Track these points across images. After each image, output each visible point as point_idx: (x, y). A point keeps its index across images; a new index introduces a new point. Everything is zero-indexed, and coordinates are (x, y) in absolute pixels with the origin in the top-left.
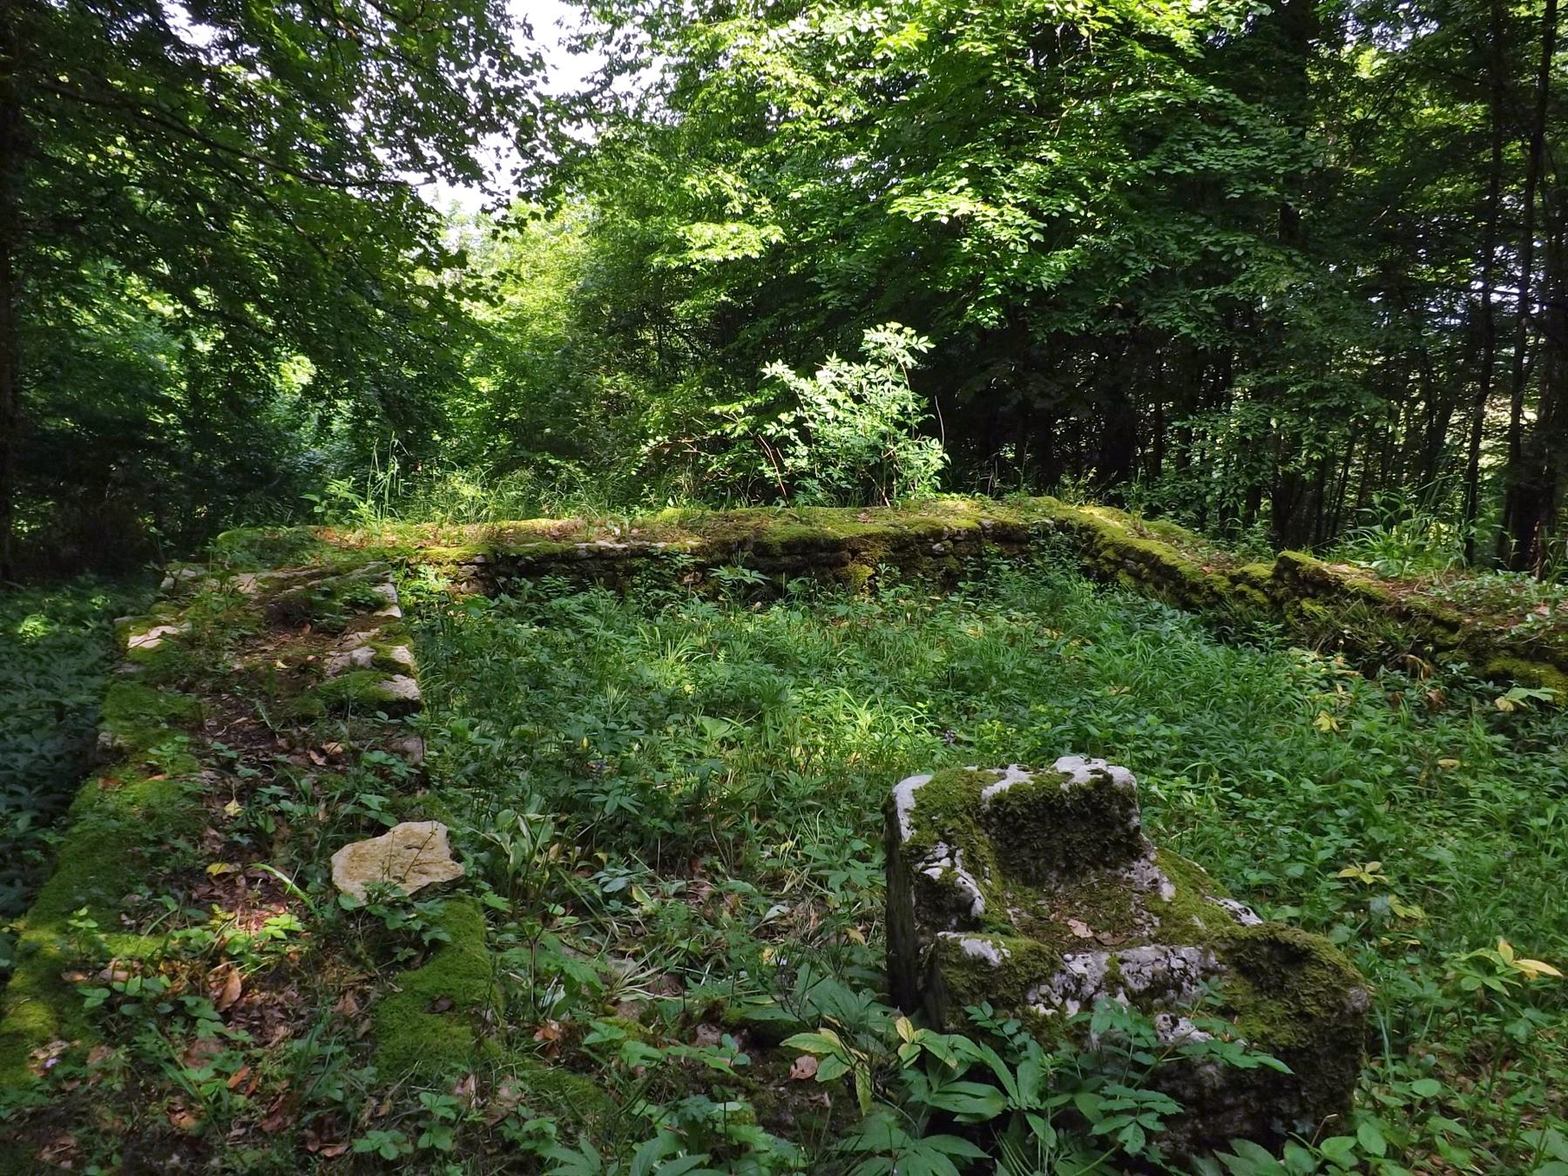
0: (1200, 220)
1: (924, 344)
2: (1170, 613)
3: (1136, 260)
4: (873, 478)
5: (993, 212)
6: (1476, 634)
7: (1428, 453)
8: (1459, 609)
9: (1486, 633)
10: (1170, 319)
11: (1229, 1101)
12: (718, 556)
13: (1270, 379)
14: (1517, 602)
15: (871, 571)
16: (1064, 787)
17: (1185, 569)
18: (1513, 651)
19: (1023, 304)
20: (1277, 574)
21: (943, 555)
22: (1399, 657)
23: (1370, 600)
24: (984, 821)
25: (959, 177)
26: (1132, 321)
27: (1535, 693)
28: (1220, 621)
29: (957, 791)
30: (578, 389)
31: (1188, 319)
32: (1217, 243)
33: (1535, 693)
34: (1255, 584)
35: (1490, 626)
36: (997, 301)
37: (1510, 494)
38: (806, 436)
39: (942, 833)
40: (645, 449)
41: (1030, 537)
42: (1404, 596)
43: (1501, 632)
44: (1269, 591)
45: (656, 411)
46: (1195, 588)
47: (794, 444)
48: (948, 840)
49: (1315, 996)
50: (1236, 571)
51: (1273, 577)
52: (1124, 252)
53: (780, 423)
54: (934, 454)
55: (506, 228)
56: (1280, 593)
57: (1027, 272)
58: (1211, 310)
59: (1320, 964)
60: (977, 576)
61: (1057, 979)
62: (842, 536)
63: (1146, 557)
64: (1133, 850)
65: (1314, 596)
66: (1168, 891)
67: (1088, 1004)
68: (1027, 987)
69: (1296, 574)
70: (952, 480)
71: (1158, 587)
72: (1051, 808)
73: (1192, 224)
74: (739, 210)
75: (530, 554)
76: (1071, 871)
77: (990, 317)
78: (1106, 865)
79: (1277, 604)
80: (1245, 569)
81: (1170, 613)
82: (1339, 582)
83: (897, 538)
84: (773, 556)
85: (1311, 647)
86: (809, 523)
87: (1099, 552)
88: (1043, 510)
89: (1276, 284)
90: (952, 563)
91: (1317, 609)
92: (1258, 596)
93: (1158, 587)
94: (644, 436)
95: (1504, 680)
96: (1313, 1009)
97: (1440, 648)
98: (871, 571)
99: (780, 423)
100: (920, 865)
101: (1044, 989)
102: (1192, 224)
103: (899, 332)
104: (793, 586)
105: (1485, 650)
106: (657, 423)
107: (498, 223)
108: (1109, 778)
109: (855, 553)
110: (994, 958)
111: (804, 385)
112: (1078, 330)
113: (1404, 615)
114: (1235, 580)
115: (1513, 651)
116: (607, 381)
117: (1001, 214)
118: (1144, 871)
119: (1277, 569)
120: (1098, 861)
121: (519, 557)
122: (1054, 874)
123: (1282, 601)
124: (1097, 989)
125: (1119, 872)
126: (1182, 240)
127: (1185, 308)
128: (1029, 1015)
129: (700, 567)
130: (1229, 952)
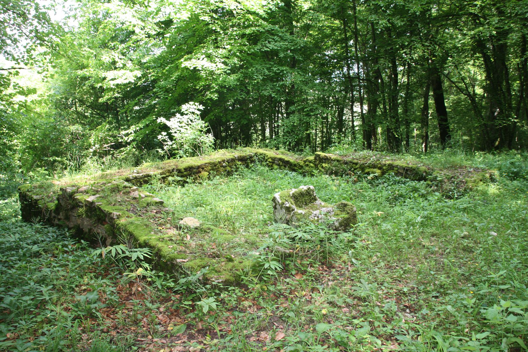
0: (272, 63)
3: (257, 76)
4: (196, 149)
5: (214, 65)
7: (340, 124)
12: (167, 174)
14: (369, 156)
18: (369, 167)
19: (224, 91)
20: (315, 159)
21: (226, 166)
22: (346, 173)
23: (338, 161)
25: (202, 55)
29: (287, 194)
31: (274, 92)
32: (278, 69)
34: (310, 162)
35: (364, 162)
36: (217, 91)
37: (364, 133)
41: (248, 158)
42: (345, 159)
44: (314, 163)
46: (295, 165)
50: (305, 159)
52: (253, 73)
53: (162, 135)
55: (47, 78)
58: (279, 89)
62: (199, 164)
63: (280, 159)
64: (316, 200)
65: (325, 162)
67: (318, 217)
70: (216, 146)
71: (285, 167)
73: (270, 64)
74: (121, 66)
76: (306, 204)
77: (215, 97)
80: (307, 158)
82: (330, 158)
83: (214, 163)
84: (182, 173)
85: (326, 174)
88: (248, 151)
89: (292, 77)
90: (228, 169)
92: (312, 165)
93: (285, 167)
94: (90, 146)
95: (368, 174)
96: (349, 212)
98: (208, 173)
99: (162, 135)
102: (270, 64)
107: (44, 77)
111: (168, 123)
112: (242, 98)
113: (346, 163)
114: (305, 162)
115: (369, 167)
117: (217, 66)
119: (315, 157)
120: (310, 202)
123: (318, 165)
126: (269, 69)
127: (271, 89)
129: (163, 178)
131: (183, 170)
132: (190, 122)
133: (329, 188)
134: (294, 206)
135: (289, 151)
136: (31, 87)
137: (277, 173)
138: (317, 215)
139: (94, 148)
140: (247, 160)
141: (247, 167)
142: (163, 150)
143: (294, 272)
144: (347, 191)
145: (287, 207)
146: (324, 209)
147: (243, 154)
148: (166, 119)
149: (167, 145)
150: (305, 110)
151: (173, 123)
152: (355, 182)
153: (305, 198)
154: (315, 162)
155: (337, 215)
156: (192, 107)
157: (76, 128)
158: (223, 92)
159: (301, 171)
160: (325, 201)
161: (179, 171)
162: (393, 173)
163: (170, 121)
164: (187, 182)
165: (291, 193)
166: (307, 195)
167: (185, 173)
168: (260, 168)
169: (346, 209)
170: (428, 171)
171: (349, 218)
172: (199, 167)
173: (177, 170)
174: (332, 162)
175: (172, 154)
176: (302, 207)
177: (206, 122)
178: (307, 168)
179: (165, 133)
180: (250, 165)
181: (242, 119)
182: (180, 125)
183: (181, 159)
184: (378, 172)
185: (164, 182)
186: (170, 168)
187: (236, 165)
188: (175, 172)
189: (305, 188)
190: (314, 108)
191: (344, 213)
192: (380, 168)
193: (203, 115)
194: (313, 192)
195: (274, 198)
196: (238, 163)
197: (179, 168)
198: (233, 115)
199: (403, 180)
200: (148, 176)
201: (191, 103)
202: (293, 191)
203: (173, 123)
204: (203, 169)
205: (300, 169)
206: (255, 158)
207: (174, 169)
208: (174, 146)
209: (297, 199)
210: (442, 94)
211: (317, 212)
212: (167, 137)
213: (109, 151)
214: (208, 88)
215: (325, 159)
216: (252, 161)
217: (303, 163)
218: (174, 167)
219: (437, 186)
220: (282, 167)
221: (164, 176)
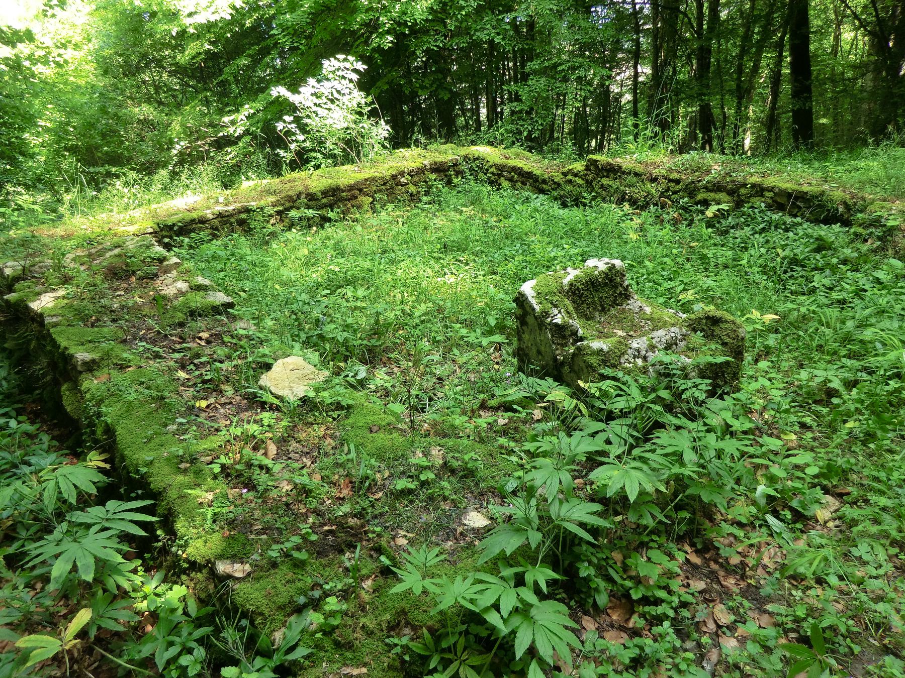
1: (366, 67)
2: (535, 196)
4: (351, 149)
6: (689, 184)
8: (679, 172)
9: (693, 182)
10: (489, 35)
12: (287, 205)
13: (546, 64)
15: (371, 199)
16: (596, 273)
17: (538, 172)
20: (587, 168)
21: (407, 184)
23: (637, 174)
26: (468, 37)
27: (721, 207)
28: (561, 197)
29: (554, 286)
31: (498, 34)
33: (721, 207)
38: (303, 129)
39: (552, 304)
40: (174, 152)
41: (449, 167)
43: (700, 181)
45: (176, 127)
46: (544, 182)
47: (294, 134)
48: (556, 306)
50: (565, 170)
51: (586, 170)
53: (284, 122)
54: (383, 130)
55: (51, 7)
57: (405, 13)
59: (727, 322)
60: (427, 193)
61: (630, 352)
62: (352, 182)
63: (513, 169)
64: (627, 297)
65: (608, 177)
66: (648, 310)
67: (645, 358)
68: (620, 357)
70: (398, 140)
72: (592, 283)
75: (179, 222)
76: (603, 310)
78: (617, 305)
79: (589, 183)
80: (570, 167)
81: (535, 196)
82: (620, 168)
84: (317, 200)
86: (330, 177)
87: (487, 170)
90: (412, 188)
91: (610, 183)
92: (579, 181)
93: (523, 183)
95: (706, 203)
96: (728, 340)
98: (371, 199)
100: (549, 319)
101: (626, 356)
103: (345, 60)
106: (178, 133)
108: (613, 265)
109: (360, 190)
110: (606, 348)
112: (438, 46)
113: (654, 180)
115: (707, 189)
116: (137, 110)
118: (635, 303)
120: (615, 304)
121: (174, 225)
122: (597, 313)
123: (591, 182)
124: (647, 351)
125: (624, 307)
127: (494, 27)
128: (624, 368)
129: (279, 213)
130: (690, 325)
131: (319, 195)
132: (336, 95)
136: (21, 27)
139: (178, 147)
140: (448, 170)
141: (449, 183)
145: (556, 325)
147: (441, 158)
148: (288, 89)
149: (296, 141)
150: (559, 69)
151: (304, 97)
156: (342, 65)
157: (146, 111)
158: (404, 34)
159: (556, 194)
161: (311, 197)
162: (763, 205)
163: (299, 93)
164: (329, 220)
166: (606, 285)
167: (325, 201)
169: (717, 331)
170: (850, 202)
172: (351, 188)
173: (308, 195)
175: (301, 160)
177: (368, 95)
178: (569, 188)
179: (292, 118)
180: (455, 181)
181: (439, 90)
182: (318, 101)
183: (319, 171)
185: (281, 220)
186: (293, 193)
187: (425, 181)
188: (303, 200)
190: (577, 64)
192: (731, 193)
193: (365, 83)
195: (521, 295)
196: (430, 176)
197: (311, 191)
198: (423, 82)
199: (789, 220)
200: (247, 210)
201: (341, 57)
202: (572, 275)
204: (360, 190)
206: (464, 167)
207: (300, 193)
208: (308, 144)
209: (580, 297)
210: (808, 38)
212: (293, 125)
213: (208, 152)
214: (372, 26)
215: (609, 171)
216: (459, 173)
218: (301, 189)
219: (879, 238)
220: (519, 185)
221: (281, 208)
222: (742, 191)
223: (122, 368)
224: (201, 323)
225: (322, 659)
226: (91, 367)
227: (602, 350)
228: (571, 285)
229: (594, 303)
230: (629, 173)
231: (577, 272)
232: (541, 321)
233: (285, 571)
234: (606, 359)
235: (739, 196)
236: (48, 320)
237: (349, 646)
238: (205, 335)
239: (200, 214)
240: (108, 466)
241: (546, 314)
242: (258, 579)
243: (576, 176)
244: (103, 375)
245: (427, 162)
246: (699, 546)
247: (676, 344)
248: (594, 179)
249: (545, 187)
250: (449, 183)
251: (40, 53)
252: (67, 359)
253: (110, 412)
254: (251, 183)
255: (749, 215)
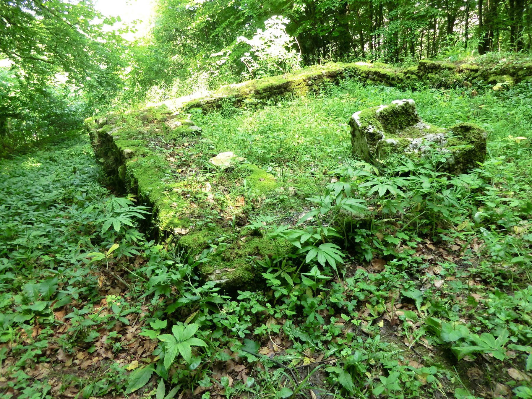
6: (484, 71)
11: (456, 167)
16: (397, 106)
18: (496, 73)
20: (419, 68)
21: (312, 85)
23: (450, 69)
24: (378, 118)
30: (163, 63)
34: (412, 73)
41: (337, 74)
46: (393, 79)
48: (371, 124)
49: (474, 137)
50: (406, 71)
54: (299, 57)
56: (421, 74)
59: (474, 129)
61: (410, 145)
62: (280, 84)
63: (375, 73)
64: (416, 121)
65: (432, 72)
67: (420, 149)
69: (425, 67)
71: (381, 81)
72: (394, 112)
76: (401, 128)
80: (409, 69)
82: (439, 66)
84: (260, 94)
91: (433, 76)
92: (414, 76)
95: (494, 83)
96: (474, 139)
97: (474, 78)
104: (269, 102)
105: (487, 75)
108: (408, 103)
110: (395, 143)
113: (461, 71)
114: (405, 73)
115: (496, 73)
119: (419, 67)
120: (408, 125)
133: (436, 104)
134: (383, 133)
135: (386, 63)
137: (372, 90)
138: (418, 146)
141: (337, 84)
142: (249, 73)
143: (369, 257)
144: (462, 108)
145: (370, 133)
146: (431, 135)
151: (255, 42)
152: (472, 96)
153: (401, 119)
154: (418, 73)
155: (452, 145)
160: (430, 121)
164: (267, 104)
165: (378, 111)
166: (403, 113)
167: (265, 94)
168: (350, 83)
169: (468, 135)
171: (474, 150)
174: (442, 71)
176: (394, 133)
177: (291, 36)
178: (408, 81)
184: (508, 80)
187: (323, 83)
189: (401, 103)
191: (465, 142)
192: (512, 75)
193: (290, 30)
194: (413, 108)
197: (257, 89)
203: (255, 42)
205: (400, 83)
209: (387, 120)
211: (417, 141)
215: (432, 69)
216: (343, 78)
217: (403, 75)
222: (520, 73)
223: (144, 156)
224: (185, 139)
225: (215, 264)
226: (131, 155)
227: (393, 144)
228: (381, 113)
229: (396, 124)
230: (445, 69)
231: (386, 107)
232: (362, 131)
233: (205, 232)
234: (394, 149)
235: (518, 76)
236: (114, 138)
237: (228, 260)
238: (186, 144)
239: (197, 102)
240: (135, 200)
241: (365, 128)
242: (191, 234)
243: (412, 73)
244: (135, 159)
245: (324, 72)
246: (435, 241)
247: (440, 142)
248: (423, 74)
249: (394, 82)
250: (337, 84)
251: (124, 27)
252: (121, 153)
253: (136, 173)
254: (225, 86)
255: (524, 87)
